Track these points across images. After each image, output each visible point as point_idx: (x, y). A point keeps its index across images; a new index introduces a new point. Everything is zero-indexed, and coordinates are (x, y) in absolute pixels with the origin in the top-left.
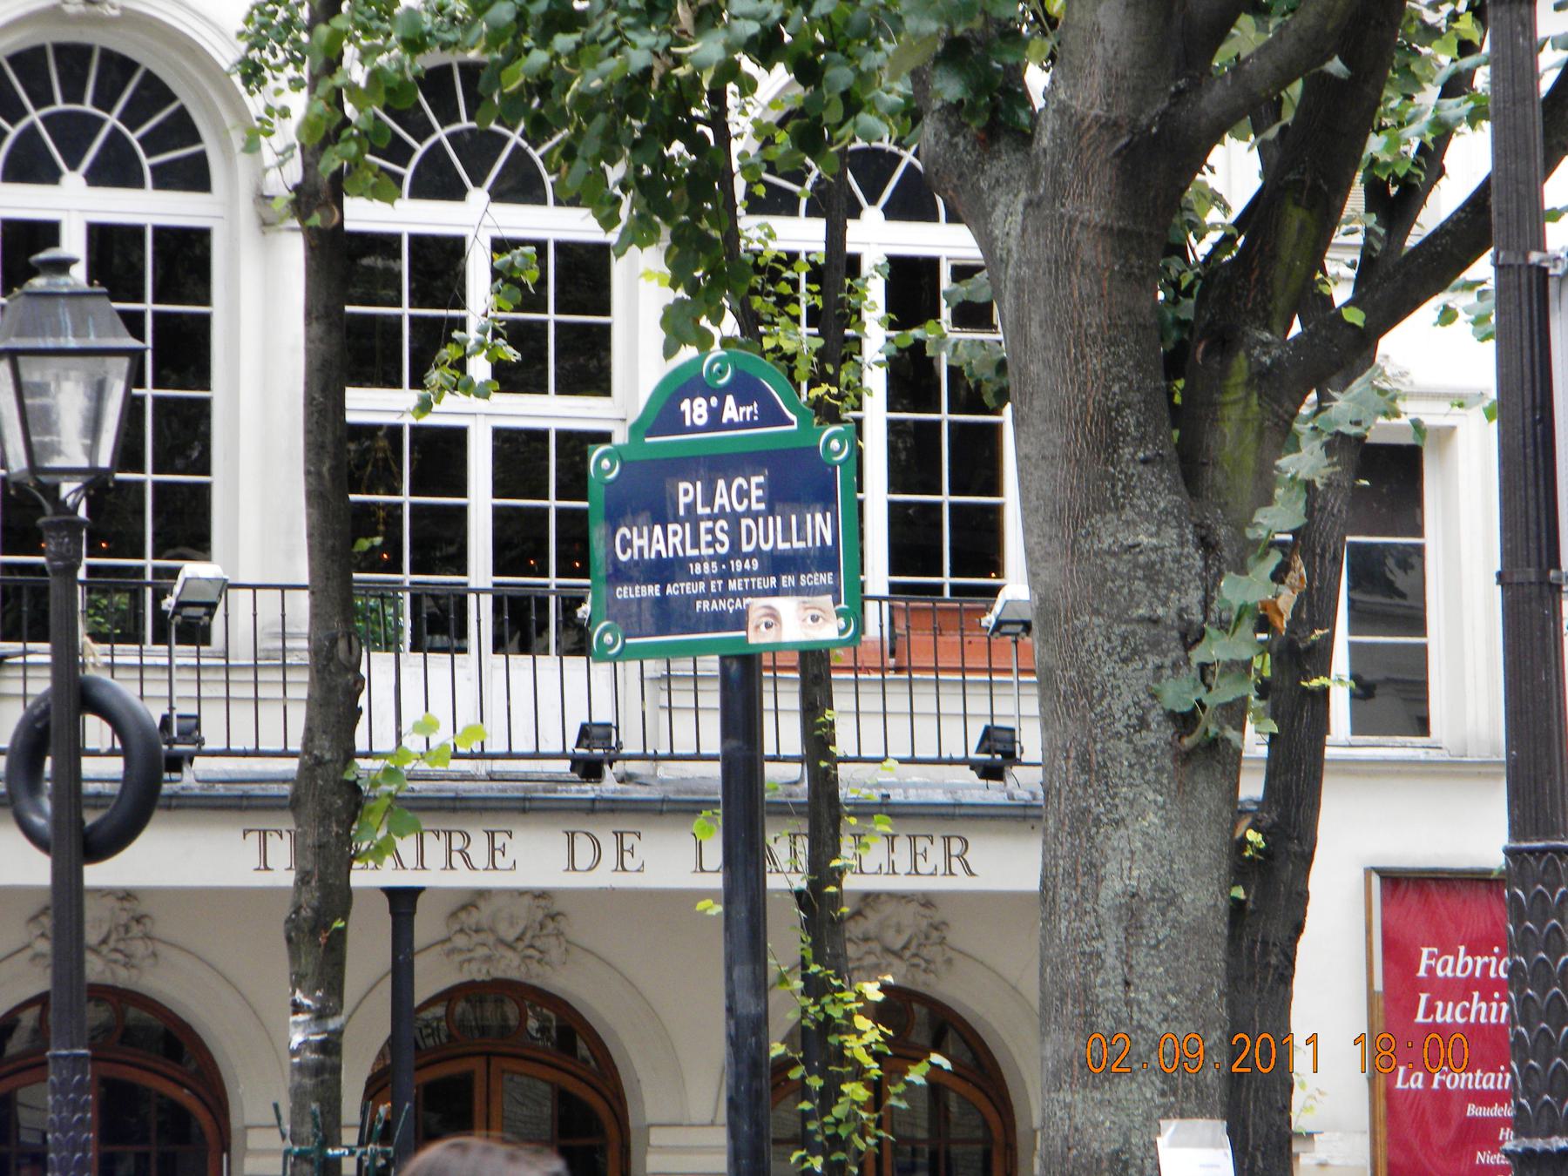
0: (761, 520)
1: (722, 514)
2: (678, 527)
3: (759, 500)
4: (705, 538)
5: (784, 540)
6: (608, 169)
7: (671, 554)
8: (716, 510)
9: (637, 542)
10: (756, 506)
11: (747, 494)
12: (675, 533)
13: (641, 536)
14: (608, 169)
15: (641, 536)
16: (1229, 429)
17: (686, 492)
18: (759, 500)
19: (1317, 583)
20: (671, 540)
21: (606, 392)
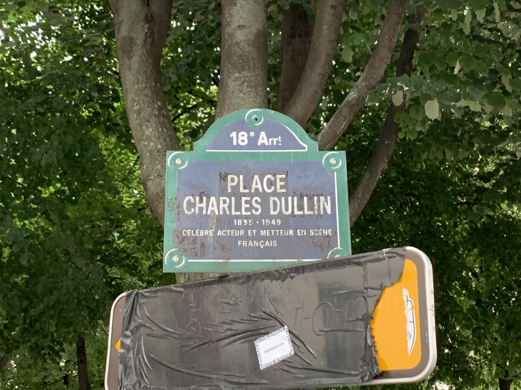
0: (283, 199)
3: (282, 187)
4: (244, 206)
8: (253, 191)
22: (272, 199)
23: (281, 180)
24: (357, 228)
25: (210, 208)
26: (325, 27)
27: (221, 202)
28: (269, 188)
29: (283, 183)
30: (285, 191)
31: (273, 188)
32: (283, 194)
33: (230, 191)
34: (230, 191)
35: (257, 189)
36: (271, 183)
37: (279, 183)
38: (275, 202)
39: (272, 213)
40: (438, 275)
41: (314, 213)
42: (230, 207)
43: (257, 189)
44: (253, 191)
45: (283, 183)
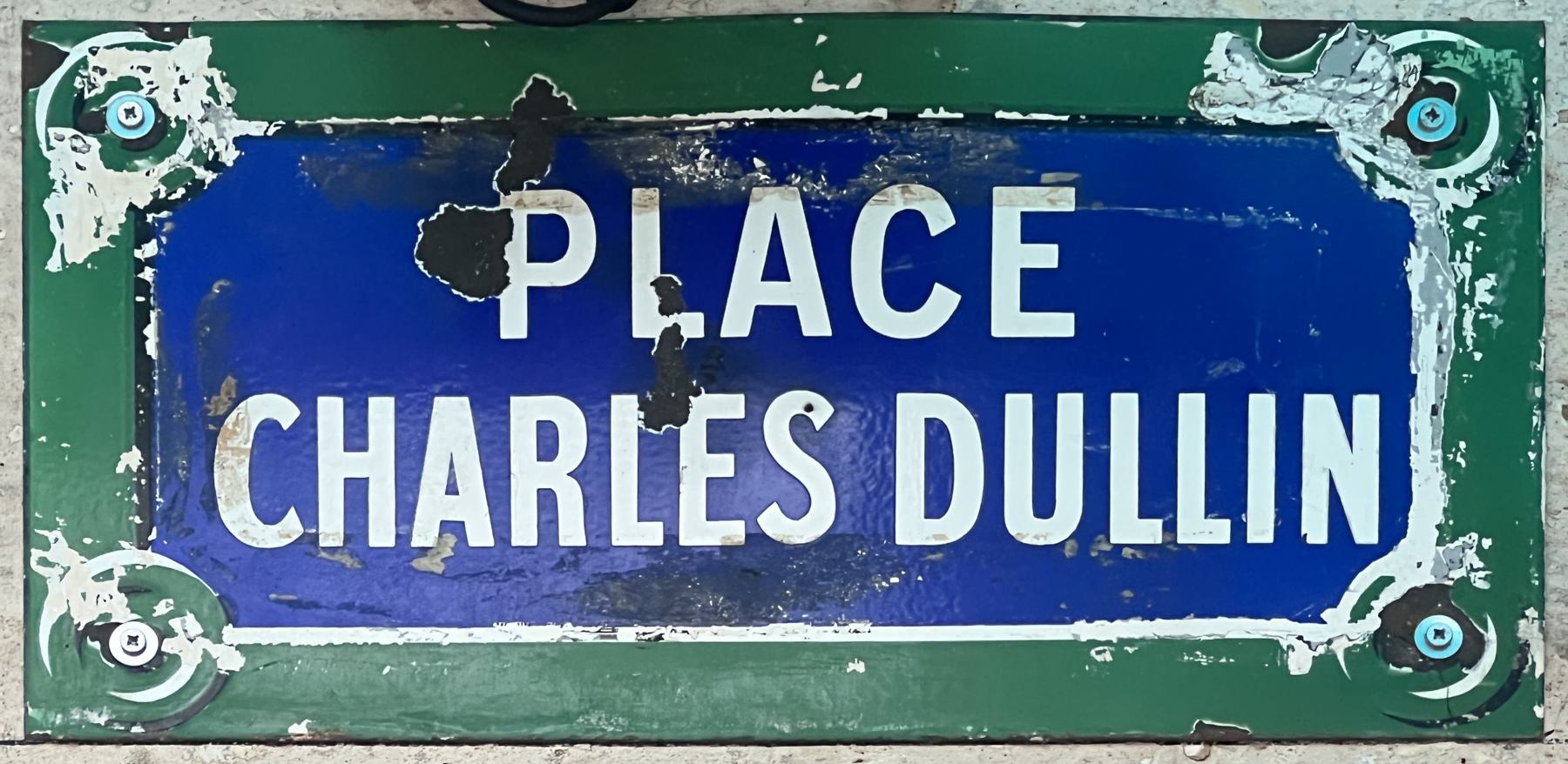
0: (1019, 408)
2: (567, 415)
3: (1038, 291)
4: (700, 463)
5: (1214, 508)
6: (208, 181)
8: (737, 323)
9: (334, 465)
10: (1010, 319)
11: (965, 260)
14: (208, 181)
15: (356, 438)
17: (549, 239)
18: (1038, 291)
20: (527, 474)
23: (1035, 228)
25: (432, 509)
27: (523, 441)
29: (1046, 256)
30: (1061, 325)
31: (942, 303)
32: (1040, 368)
33: (514, 323)
34: (514, 323)
36: (914, 263)
37: (1012, 256)
39: (913, 527)
40: (406, 436)
41: (1239, 529)
44: (737, 323)
45: (1046, 256)
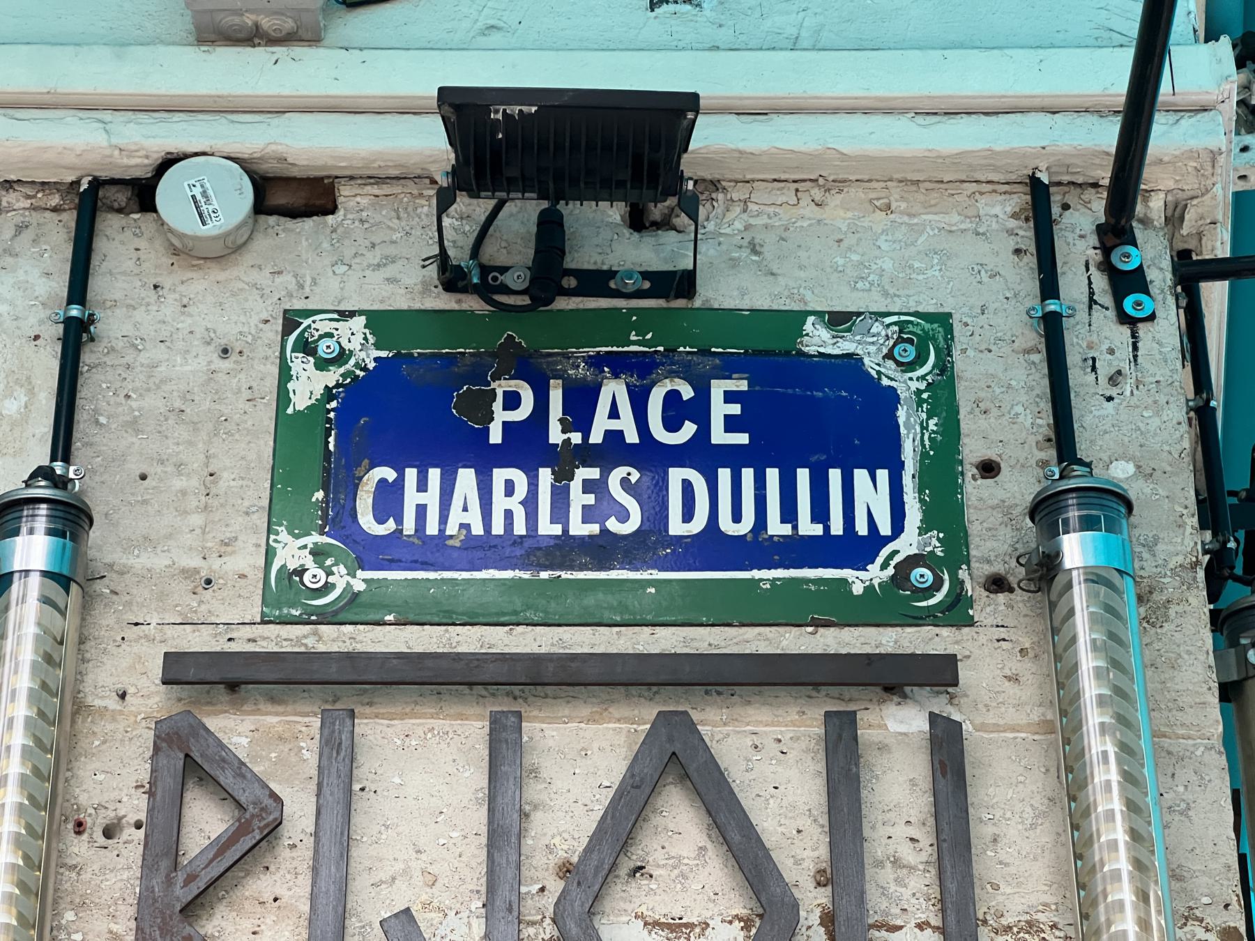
0: (724, 475)
1: (613, 451)
3: (731, 424)
7: (498, 528)
8: (596, 437)
10: (719, 435)
12: (510, 489)
13: (422, 486)
15: (422, 486)
16: (273, 720)
17: (512, 401)
18: (731, 424)
19: (313, 618)
20: (500, 503)
21: (725, 416)
22: (676, 475)
24: (10, 583)
26: (1012, 831)
28: (672, 424)
29: (735, 409)
33: (496, 436)
34: (496, 436)
35: (614, 437)
37: (720, 410)
38: (687, 487)
39: (676, 527)
41: (827, 529)
42: (530, 503)
43: (614, 437)
44: (596, 437)
45: (735, 409)
